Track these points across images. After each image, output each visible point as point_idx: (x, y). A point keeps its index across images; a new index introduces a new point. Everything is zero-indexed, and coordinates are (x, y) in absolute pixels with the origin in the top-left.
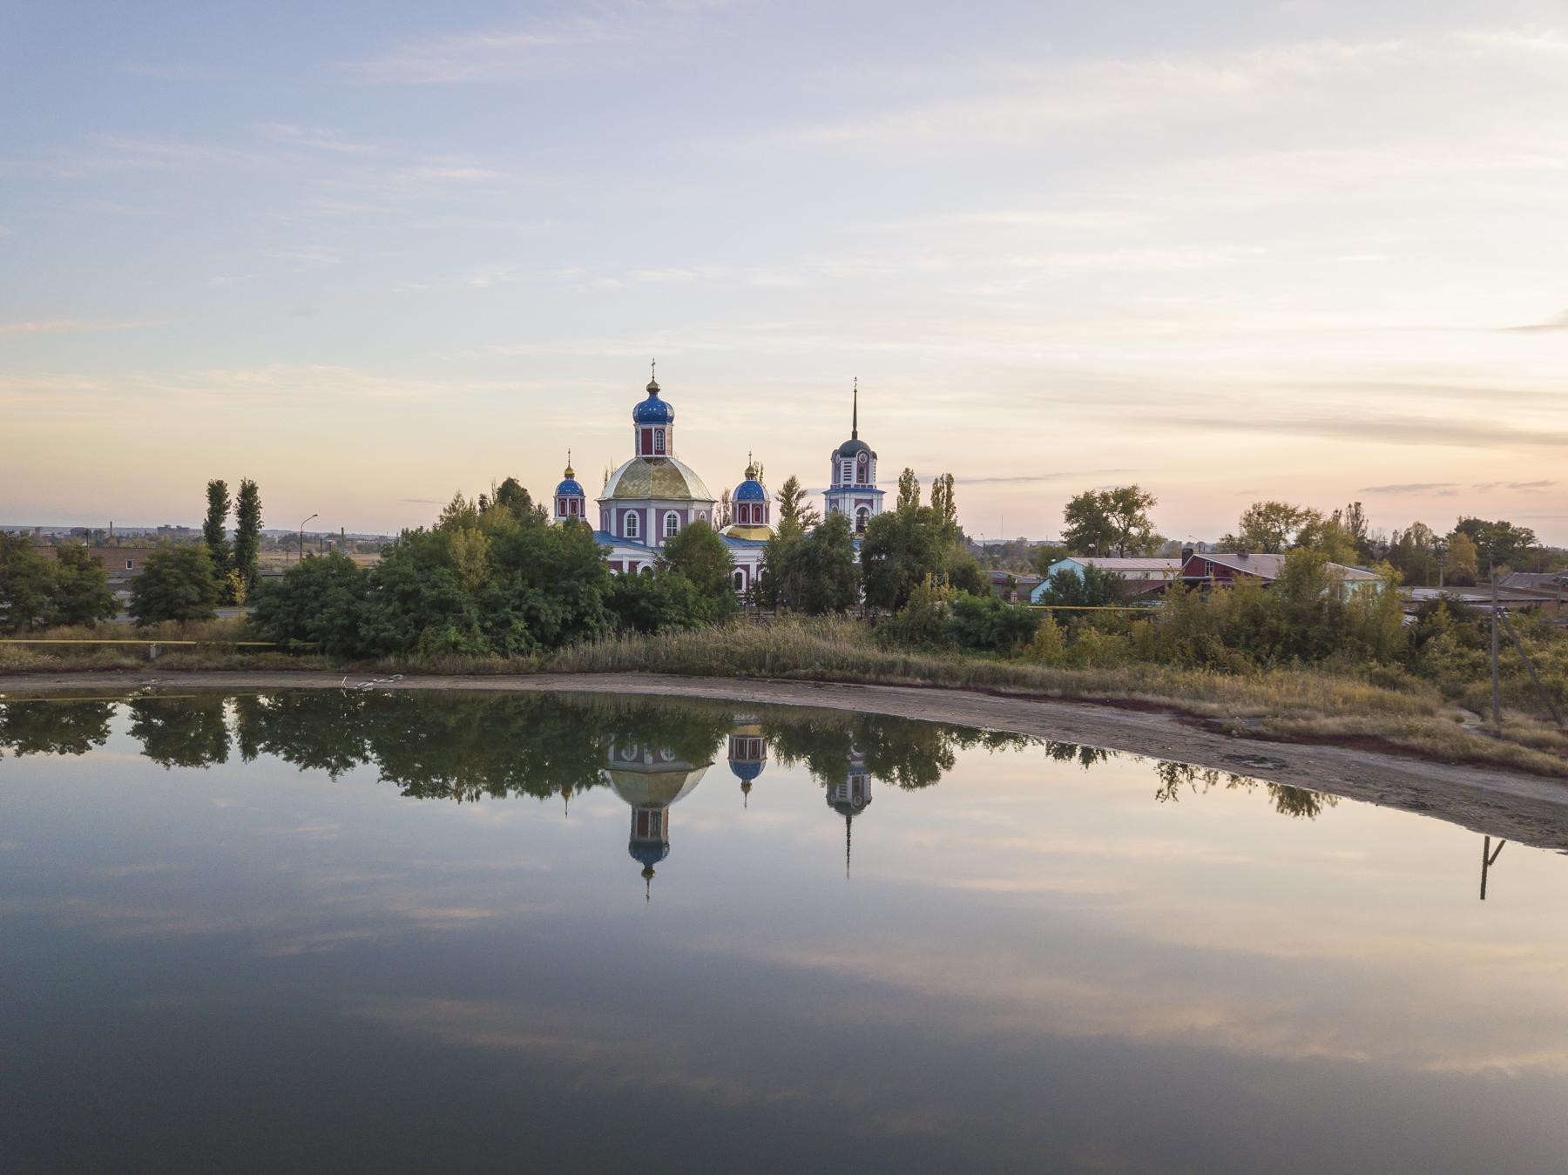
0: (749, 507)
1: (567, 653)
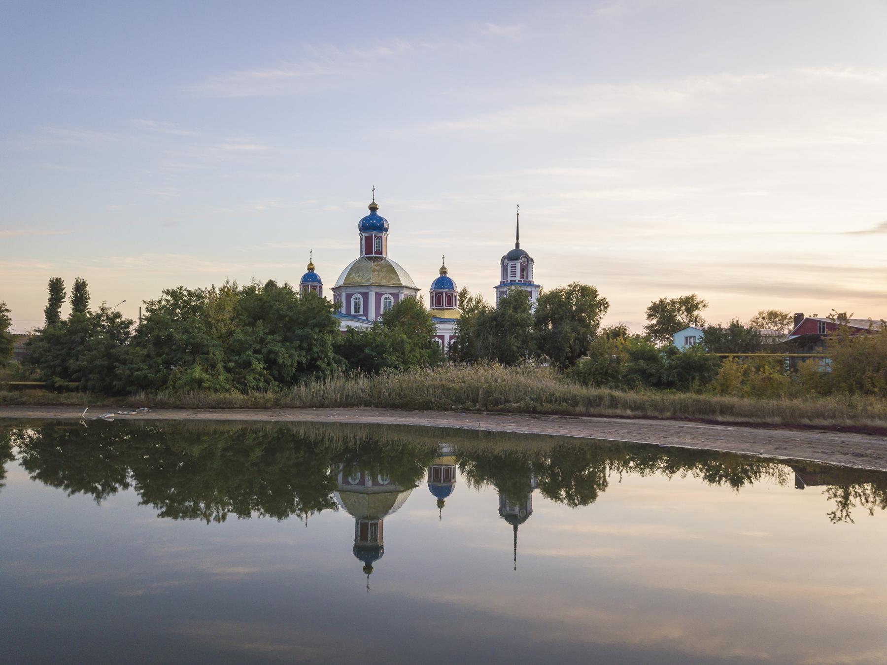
0: (443, 295)
1: (301, 390)
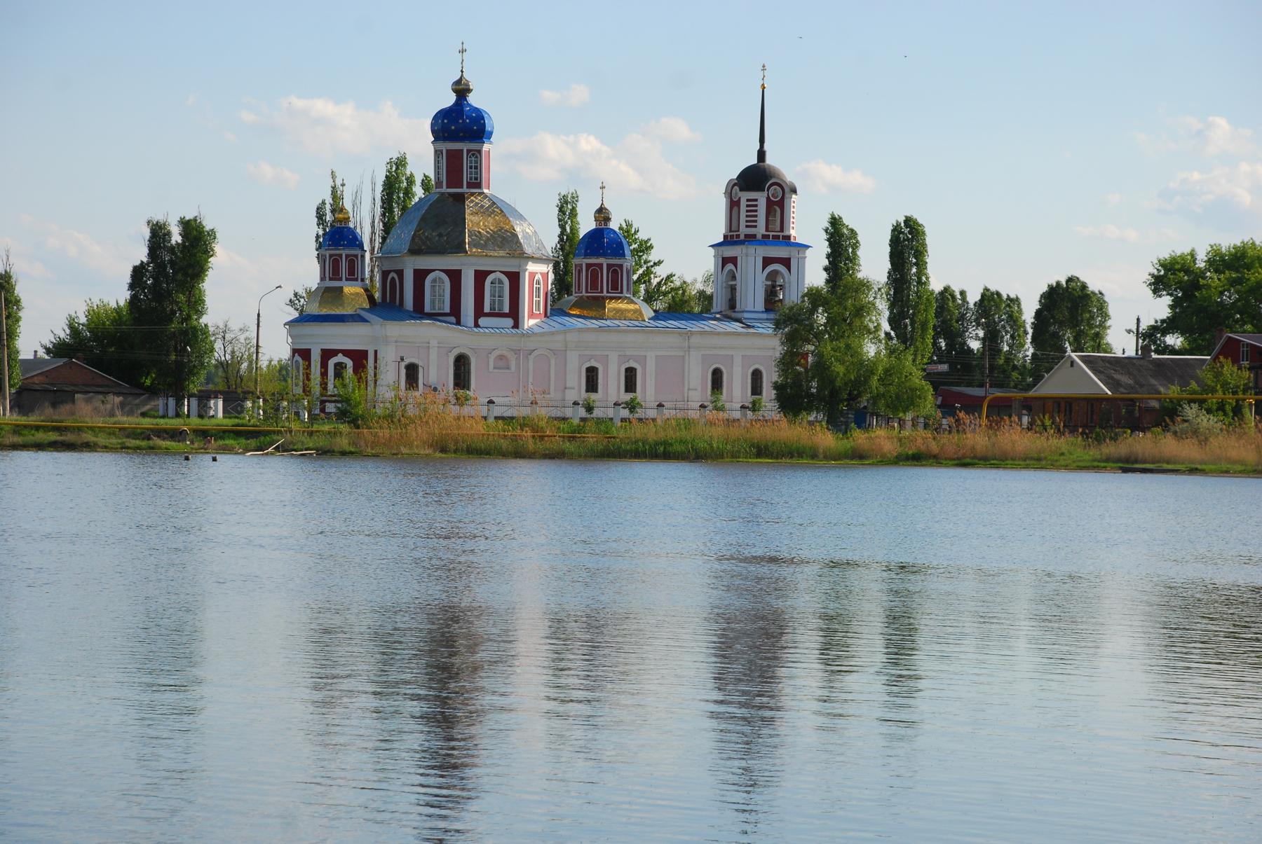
0: (341, 258)
